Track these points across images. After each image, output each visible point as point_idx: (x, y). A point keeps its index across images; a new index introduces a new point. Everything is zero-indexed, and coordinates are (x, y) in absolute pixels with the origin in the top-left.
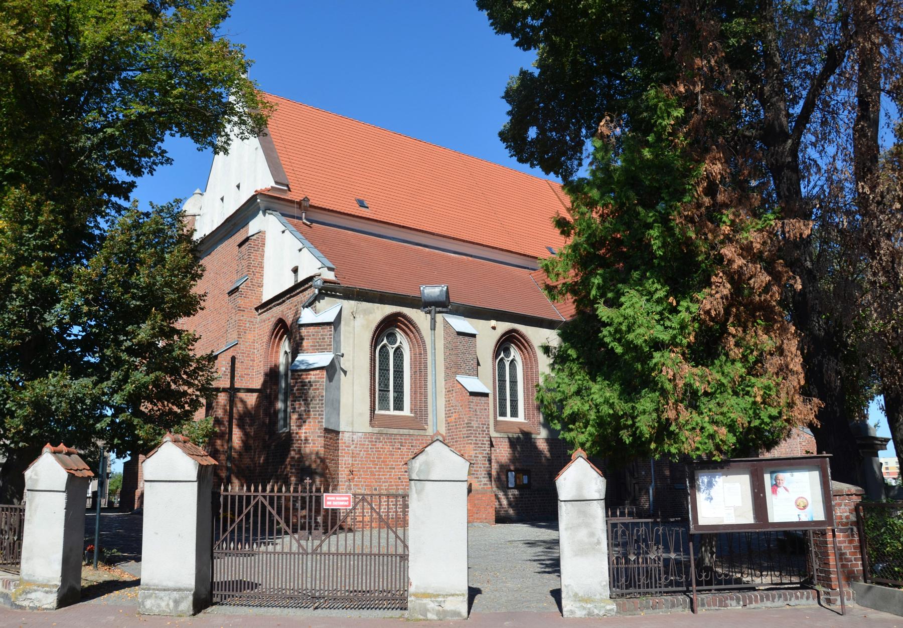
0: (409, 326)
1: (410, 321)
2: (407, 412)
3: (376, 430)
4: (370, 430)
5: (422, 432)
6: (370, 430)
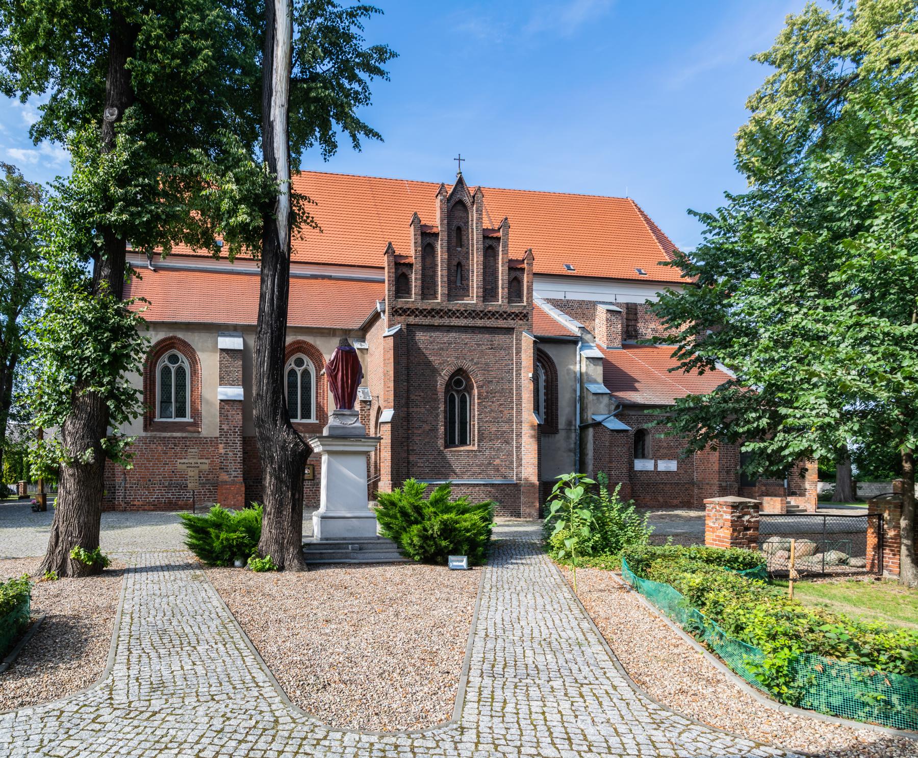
2: (313, 420)
3: (149, 434)
4: (144, 434)
6: (144, 434)
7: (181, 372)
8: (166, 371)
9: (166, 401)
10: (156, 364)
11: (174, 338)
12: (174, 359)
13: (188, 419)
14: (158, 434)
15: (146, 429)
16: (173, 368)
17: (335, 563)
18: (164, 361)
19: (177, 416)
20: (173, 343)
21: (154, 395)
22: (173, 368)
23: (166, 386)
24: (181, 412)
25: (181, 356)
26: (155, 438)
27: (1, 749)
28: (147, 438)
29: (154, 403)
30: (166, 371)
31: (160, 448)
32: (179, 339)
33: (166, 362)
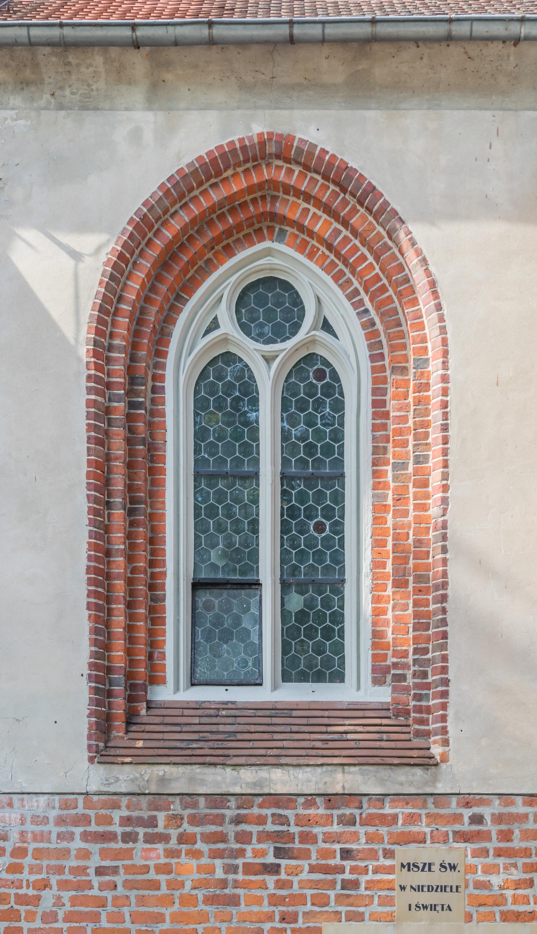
0: (350, 211)
1: (340, 176)
2: (358, 688)
3: (125, 777)
4: (94, 778)
5: (409, 780)
6: (94, 778)
7: (313, 389)
8: (224, 391)
9: (223, 584)
10: (162, 337)
11: (277, 150)
12: (270, 306)
13: (358, 688)
14: (180, 778)
15: (104, 743)
16: (267, 367)
17: (148, 764)
18: (206, 321)
19: (290, 673)
20: (270, 190)
21: (155, 540)
22: (267, 367)
23: (223, 474)
24: (313, 643)
25: (312, 281)
26: (159, 799)
27: (5, 838)
28: (112, 799)
29: (155, 586)
30: (224, 391)
31: (189, 869)
32: (309, 160)
33: (228, 326)
